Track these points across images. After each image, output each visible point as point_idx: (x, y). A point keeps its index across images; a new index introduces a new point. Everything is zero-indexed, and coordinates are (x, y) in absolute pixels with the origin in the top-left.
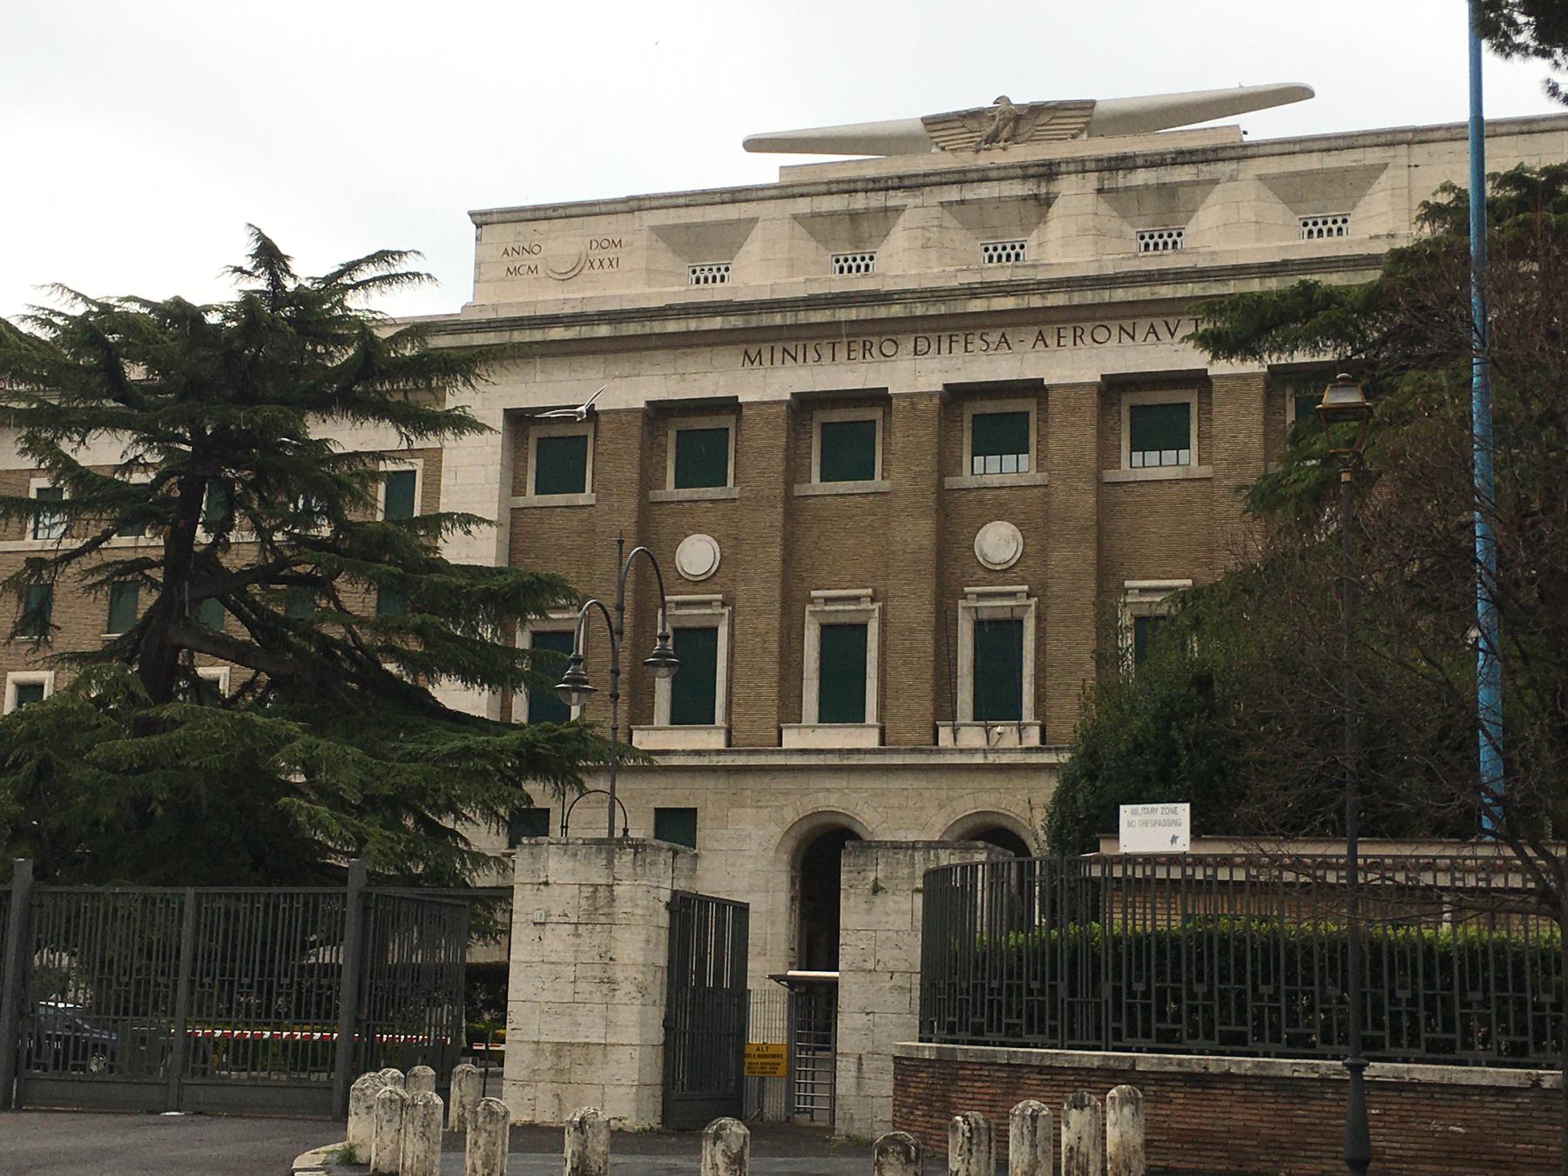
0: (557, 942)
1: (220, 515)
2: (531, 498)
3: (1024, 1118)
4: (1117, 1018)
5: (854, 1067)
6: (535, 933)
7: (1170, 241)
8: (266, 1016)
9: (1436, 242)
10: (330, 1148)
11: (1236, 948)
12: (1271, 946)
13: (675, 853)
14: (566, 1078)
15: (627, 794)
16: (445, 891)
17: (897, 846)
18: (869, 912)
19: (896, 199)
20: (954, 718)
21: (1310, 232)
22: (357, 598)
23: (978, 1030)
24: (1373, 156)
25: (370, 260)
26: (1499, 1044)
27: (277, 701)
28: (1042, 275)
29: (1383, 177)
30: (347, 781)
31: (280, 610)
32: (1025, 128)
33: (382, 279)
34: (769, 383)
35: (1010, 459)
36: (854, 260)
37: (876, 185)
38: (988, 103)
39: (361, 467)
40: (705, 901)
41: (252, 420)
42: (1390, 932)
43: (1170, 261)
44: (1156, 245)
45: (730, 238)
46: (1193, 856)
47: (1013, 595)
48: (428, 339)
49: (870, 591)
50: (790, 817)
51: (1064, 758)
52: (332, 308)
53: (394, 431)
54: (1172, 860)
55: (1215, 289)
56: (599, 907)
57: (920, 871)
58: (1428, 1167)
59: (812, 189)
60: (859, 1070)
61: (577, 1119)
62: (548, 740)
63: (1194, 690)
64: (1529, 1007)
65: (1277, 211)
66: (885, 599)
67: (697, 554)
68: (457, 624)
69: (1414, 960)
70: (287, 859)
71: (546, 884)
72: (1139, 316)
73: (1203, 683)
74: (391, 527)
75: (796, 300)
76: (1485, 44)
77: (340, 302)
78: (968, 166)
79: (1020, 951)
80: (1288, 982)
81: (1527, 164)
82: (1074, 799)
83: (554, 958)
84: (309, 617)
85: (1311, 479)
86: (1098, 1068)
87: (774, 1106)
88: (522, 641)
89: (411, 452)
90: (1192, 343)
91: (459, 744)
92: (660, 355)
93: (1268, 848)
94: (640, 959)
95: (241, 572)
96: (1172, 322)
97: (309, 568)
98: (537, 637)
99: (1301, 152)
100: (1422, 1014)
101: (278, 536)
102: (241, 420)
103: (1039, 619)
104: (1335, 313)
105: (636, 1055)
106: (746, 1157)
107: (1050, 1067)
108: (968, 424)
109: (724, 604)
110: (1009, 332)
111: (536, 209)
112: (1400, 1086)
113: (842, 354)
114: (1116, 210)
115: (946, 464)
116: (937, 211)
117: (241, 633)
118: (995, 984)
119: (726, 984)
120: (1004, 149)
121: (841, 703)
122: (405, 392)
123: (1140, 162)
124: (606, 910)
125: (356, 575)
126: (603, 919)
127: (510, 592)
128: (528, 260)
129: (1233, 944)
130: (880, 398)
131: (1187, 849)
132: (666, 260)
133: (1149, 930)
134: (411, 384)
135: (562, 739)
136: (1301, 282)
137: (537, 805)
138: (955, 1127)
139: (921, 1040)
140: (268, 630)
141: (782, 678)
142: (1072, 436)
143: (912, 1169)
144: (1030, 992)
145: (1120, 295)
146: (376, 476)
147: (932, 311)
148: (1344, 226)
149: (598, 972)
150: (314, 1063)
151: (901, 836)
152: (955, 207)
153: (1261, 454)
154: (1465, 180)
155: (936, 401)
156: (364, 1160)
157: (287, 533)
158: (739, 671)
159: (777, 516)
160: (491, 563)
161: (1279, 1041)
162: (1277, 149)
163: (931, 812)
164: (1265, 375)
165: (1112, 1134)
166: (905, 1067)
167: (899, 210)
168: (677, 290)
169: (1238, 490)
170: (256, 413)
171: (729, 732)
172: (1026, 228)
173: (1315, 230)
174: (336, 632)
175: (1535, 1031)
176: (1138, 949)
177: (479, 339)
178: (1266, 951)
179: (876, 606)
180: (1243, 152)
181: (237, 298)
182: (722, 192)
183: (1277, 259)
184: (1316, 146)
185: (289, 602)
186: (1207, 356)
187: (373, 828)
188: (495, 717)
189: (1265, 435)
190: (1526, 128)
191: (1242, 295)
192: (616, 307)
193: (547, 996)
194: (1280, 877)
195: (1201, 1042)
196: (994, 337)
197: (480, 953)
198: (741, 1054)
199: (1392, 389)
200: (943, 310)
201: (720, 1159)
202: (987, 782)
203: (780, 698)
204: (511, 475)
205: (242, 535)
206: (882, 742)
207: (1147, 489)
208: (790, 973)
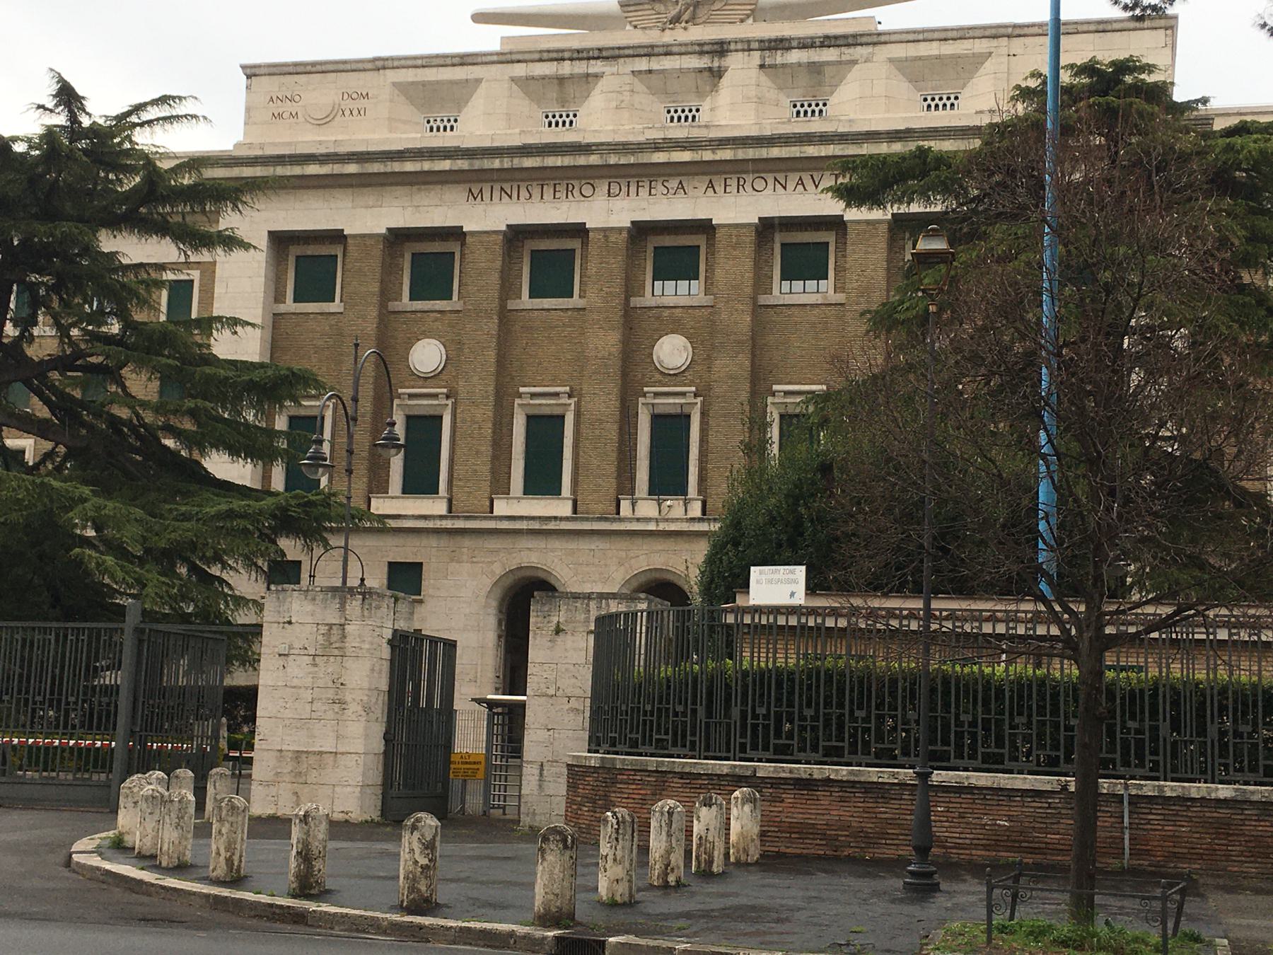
1: (26, 312)
2: (289, 305)
3: (662, 814)
4: (743, 735)
5: (537, 772)
6: (281, 662)
7: (817, 110)
8: (54, 728)
9: (1026, 118)
10: (103, 835)
11: (839, 682)
12: (864, 682)
13: (396, 600)
15: (365, 550)
16: (214, 628)
17: (576, 596)
19: (596, 67)
20: (633, 494)
21: (929, 106)
22: (141, 384)
23: (634, 744)
24: (981, 46)
25: (155, 102)
26: (1038, 756)
27: (73, 468)
28: (713, 134)
29: (987, 64)
30: (130, 536)
31: (77, 394)
33: (164, 119)
34: (489, 216)
36: (561, 116)
37: (580, 55)
39: (145, 276)
41: (52, 235)
42: (958, 668)
43: (816, 126)
44: (806, 112)
45: (461, 93)
46: (807, 608)
47: (683, 394)
48: (203, 170)
49: (567, 389)
50: (498, 570)
51: (715, 527)
52: (121, 143)
53: (173, 246)
55: (852, 150)
56: (333, 642)
57: (594, 613)
58: (979, 853)
59: (527, 57)
60: (541, 775)
61: (302, 813)
64: (1062, 729)
65: (902, 87)
66: (580, 396)
67: (427, 355)
68: (224, 408)
69: (976, 691)
70: (86, 602)
71: (290, 623)
72: (670, 175)
73: (826, 469)
74: (171, 327)
75: (509, 148)
77: (129, 138)
79: (668, 681)
80: (877, 708)
81: (1099, 58)
83: (296, 682)
84: (100, 399)
86: (727, 775)
87: (474, 802)
88: (281, 424)
89: (187, 264)
90: (830, 194)
91: (224, 507)
92: (400, 190)
93: (857, 602)
94: (366, 685)
95: (42, 361)
96: (817, 176)
97: (100, 359)
98: (292, 419)
99: (924, 40)
100: (981, 733)
101: (75, 332)
102: (43, 233)
103: (704, 414)
104: (944, 173)
105: (361, 762)
106: (438, 844)
107: (690, 773)
109: (448, 397)
111: (296, 64)
112: (960, 790)
113: (549, 192)
114: (774, 82)
115: (631, 287)
117: (43, 412)
119: (437, 705)
120: (685, 29)
121: (542, 479)
123: (794, 44)
124: (337, 645)
125: (141, 364)
126: (336, 652)
127: (271, 384)
128: (288, 107)
130: (579, 231)
131: (802, 602)
132: (407, 111)
133: (770, 666)
134: (188, 208)
135: (310, 504)
136: (919, 148)
137: (289, 558)
138: (606, 820)
139: (589, 751)
140: (64, 407)
141: (495, 458)
142: (733, 267)
143: (568, 853)
144: (676, 714)
145: (775, 152)
146: (159, 284)
148: (956, 102)
149: (330, 694)
150: (95, 767)
151: (587, 589)
154: (1046, 70)
155: (625, 234)
156: (129, 845)
157: (83, 329)
158: (458, 452)
159: (492, 325)
160: (256, 358)
161: (869, 753)
162: (905, 37)
164: (888, 222)
166: (576, 773)
167: (597, 76)
168: (414, 136)
169: (862, 314)
170: (55, 228)
171: (450, 501)
172: (701, 94)
173: (933, 105)
175: (1065, 747)
177: (248, 172)
178: (861, 682)
179: (572, 401)
180: (877, 39)
181: (40, 130)
183: (902, 128)
185: (85, 387)
186: (842, 204)
187: (152, 575)
189: (888, 269)
190: (1101, 27)
191: (871, 156)
193: (288, 714)
195: (859, 757)
196: (673, 183)
197: (238, 678)
198: (448, 761)
199: (984, 236)
200: (632, 160)
201: (416, 846)
202: (659, 545)
204: (273, 287)
205: (44, 329)
206: (575, 511)
208: (489, 697)
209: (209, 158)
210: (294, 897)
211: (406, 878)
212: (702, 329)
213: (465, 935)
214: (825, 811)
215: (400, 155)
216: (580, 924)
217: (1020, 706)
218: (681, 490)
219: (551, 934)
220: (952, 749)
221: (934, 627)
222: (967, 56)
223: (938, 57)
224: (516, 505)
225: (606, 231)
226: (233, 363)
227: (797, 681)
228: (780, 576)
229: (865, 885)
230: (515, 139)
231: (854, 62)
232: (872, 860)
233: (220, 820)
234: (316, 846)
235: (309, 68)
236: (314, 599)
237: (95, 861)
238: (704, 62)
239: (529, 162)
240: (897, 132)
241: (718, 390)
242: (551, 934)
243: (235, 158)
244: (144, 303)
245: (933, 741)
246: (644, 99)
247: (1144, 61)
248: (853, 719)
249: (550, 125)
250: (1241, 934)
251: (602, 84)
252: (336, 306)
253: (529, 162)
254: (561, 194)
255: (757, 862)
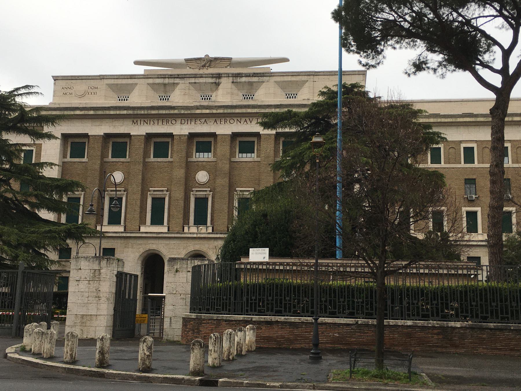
0: (83, 286)
2: (68, 159)
4: (247, 306)
6: (77, 283)
10: (18, 346)
12: (289, 286)
14: (84, 325)
18: (174, 277)
19: (177, 81)
20: (207, 225)
23: (208, 310)
24: (304, 78)
25: (23, 87)
28: (217, 104)
29: (307, 84)
30: (13, 239)
32: (213, 63)
34: (140, 130)
35: (206, 154)
37: (171, 76)
38: (203, 56)
40: (126, 274)
43: (251, 102)
45: (129, 89)
47: (206, 191)
50: (142, 250)
51: (226, 236)
52: (11, 101)
54: (261, 263)
55: (263, 111)
56: (96, 276)
60: (171, 321)
62: (74, 228)
63: (262, 218)
65: (279, 91)
66: (170, 191)
67: (118, 176)
71: (80, 269)
72: (155, 118)
73: (265, 216)
75: (147, 107)
76: (343, 49)
77: (14, 99)
78: (197, 73)
80: (441, 300)
82: (229, 246)
83: (82, 290)
85: (289, 163)
88: (65, 199)
91: (48, 229)
92: (107, 120)
94: (108, 291)
98: (69, 198)
103: (213, 198)
105: (106, 318)
108: (195, 144)
109: (124, 191)
110: (217, 119)
111: (72, 76)
115: (188, 155)
116: (188, 85)
118: (213, 297)
121: (157, 220)
122: (33, 127)
123: (243, 75)
126: (97, 279)
127: (63, 185)
128: (69, 91)
129: (279, 286)
130: (171, 135)
132: (111, 93)
138: (211, 337)
141: (141, 212)
142: (223, 148)
143: (202, 349)
144: (223, 299)
145: (237, 111)
146: (22, 151)
147: (186, 112)
149: (95, 294)
152: (193, 84)
153: (273, 155)
158: (128, 210)
160: (56, 177)
162: (280, 74)
163: (182, 250)
165: (248, 338)
166: (186, 321)
167: (177, 84)
168: (113, 102)
172: (212, 91)
174: (9, 195)
176: (254, 289)
177: (54, 113)
179: (168, 193)
180: (271, 75)
182: (127, 75)
183: (279, 104)
184: (290, 74)
188: (56, 221)
192: (95, 106)
194: (275, 267)
195: (269, 313)
196: (203, 120)
200: (189, 112)
201: (145, 348)
202: (197, 242)
203: (140, 218)
207: (235, 164)
209: (44, 108)
210: (98, 368)
211: (141, 360)
212: (212, 169)
213: (166, 380)
214: (276, 332)
215: (109, 108)
216: (206, 374)
217: (342, 295)
218: (205, 223)
219: (198, 378)
220: (283, 309)
221: (385, 269)
222: (300, 81)
223: (290, 81)
224: (148, 228)
225: (180, 136)
226: (50, 179)
227: (266, 288)
228: (260, 251)
229: (297, 358)
230: (148, 103)
231: (263, 82)
232: (292, 348)
233: (68, 340)
234: (106, 349)
235: (77, 78)
236: (89, 261)
237: (17, 356)
238: (213, 80)
239: (153, 112)
240: (278, 105)
241: (218, 190)
242: (198, 378)
243: (50, 108)
244: (18, 157)
245: (207, 306)
246: (193, 92)
247: (361, 84)
248: (285, 300)
249: (161, 99)
250: (428, 372)
251: (179, 87)
252: (85, 160)
253: (153, 112)
254: (165, 123)
255: (255, 351)
